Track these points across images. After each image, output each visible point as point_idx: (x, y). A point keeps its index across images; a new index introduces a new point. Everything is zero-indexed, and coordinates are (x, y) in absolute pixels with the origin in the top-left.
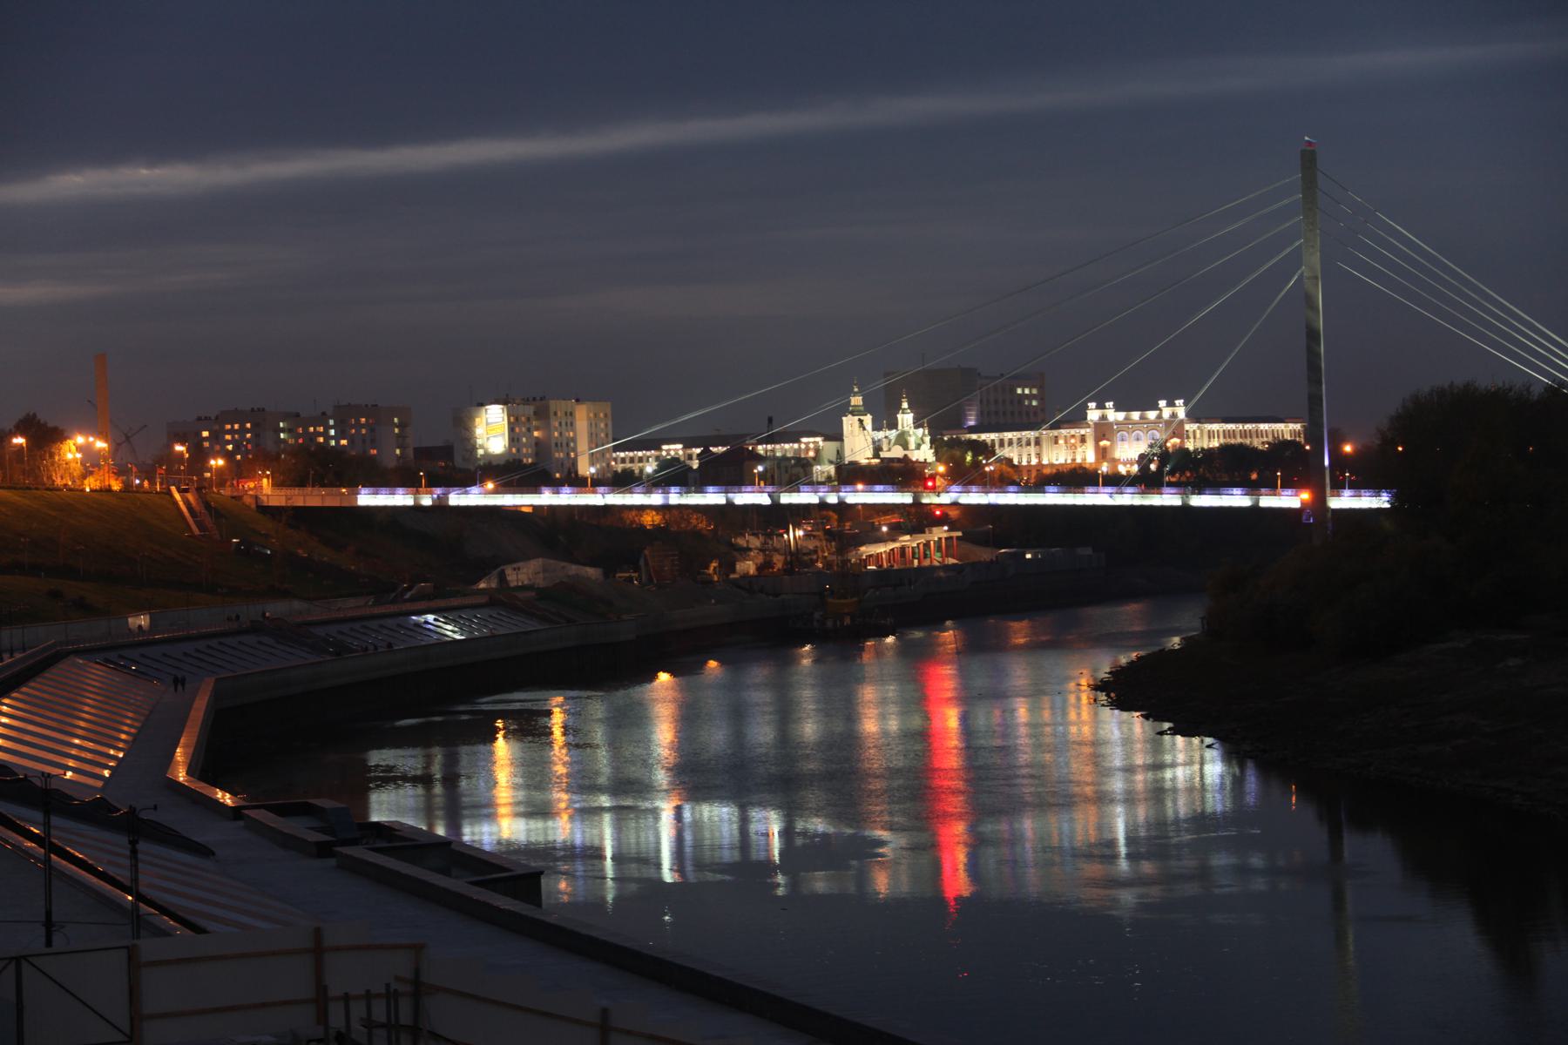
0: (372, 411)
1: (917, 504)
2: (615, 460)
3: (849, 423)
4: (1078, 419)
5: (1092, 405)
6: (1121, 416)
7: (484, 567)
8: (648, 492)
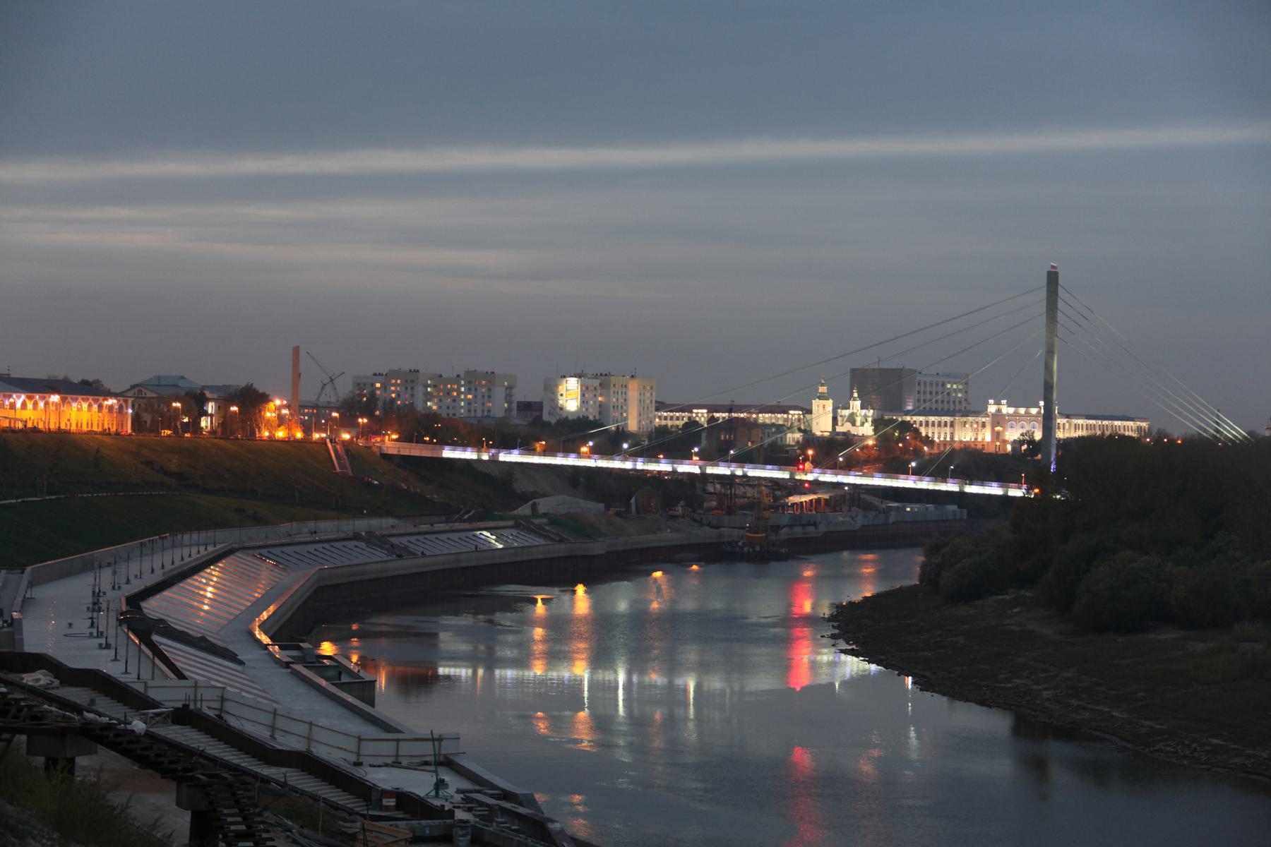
0: (490, 376)
1: (792, 478)
2: (660, 418)
3: (816, 404)
4: (981, 411)
5: (991, 401)
6: (1011, 410)
7: (524, 498)
8: (626, 460)
